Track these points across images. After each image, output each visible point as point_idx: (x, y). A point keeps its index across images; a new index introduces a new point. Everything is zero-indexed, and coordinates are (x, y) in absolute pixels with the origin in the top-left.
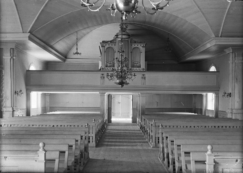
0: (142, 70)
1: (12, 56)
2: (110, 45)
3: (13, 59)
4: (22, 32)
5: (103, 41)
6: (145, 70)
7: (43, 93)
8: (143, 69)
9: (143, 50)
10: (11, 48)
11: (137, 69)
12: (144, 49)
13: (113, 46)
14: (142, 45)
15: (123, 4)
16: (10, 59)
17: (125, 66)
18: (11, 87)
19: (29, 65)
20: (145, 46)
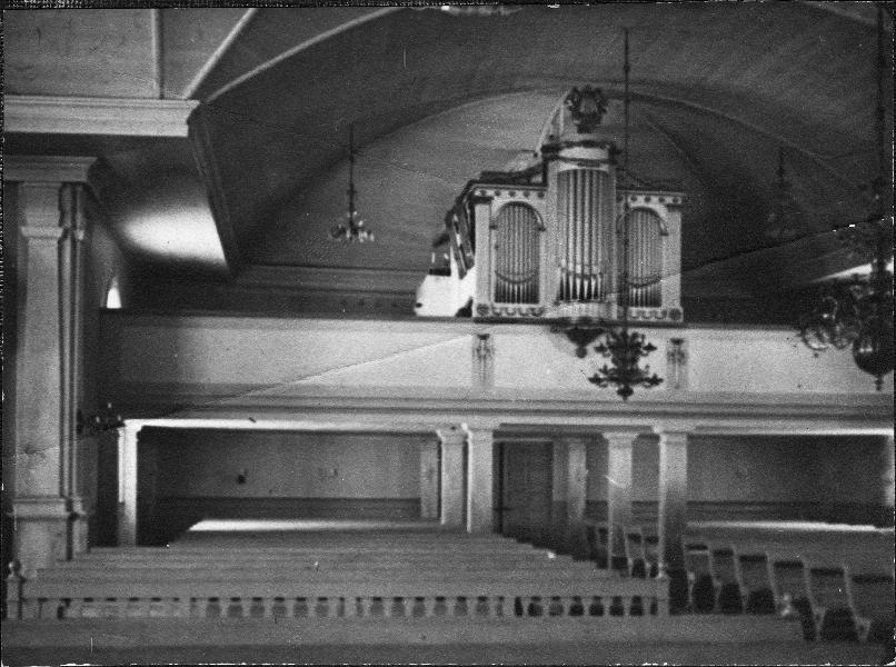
0: (668, 319)
1: (68, 224)
2: (520, 197)
3: (74, 242)
4: (157, 95)
5: (484, 174)
6: (681, 320)
7: (145, 429)
8: (674, 314)
9: (673, 222)
10: (65, 184)
11: (647, 315)
12: (678, 217)
13: (533, 200)
14: (669, 200)
15: (208, 210)
16: (61, 242)
17: (575, 297)
18: (61, 321)
19: (107, 89)
20: (680, 202)
